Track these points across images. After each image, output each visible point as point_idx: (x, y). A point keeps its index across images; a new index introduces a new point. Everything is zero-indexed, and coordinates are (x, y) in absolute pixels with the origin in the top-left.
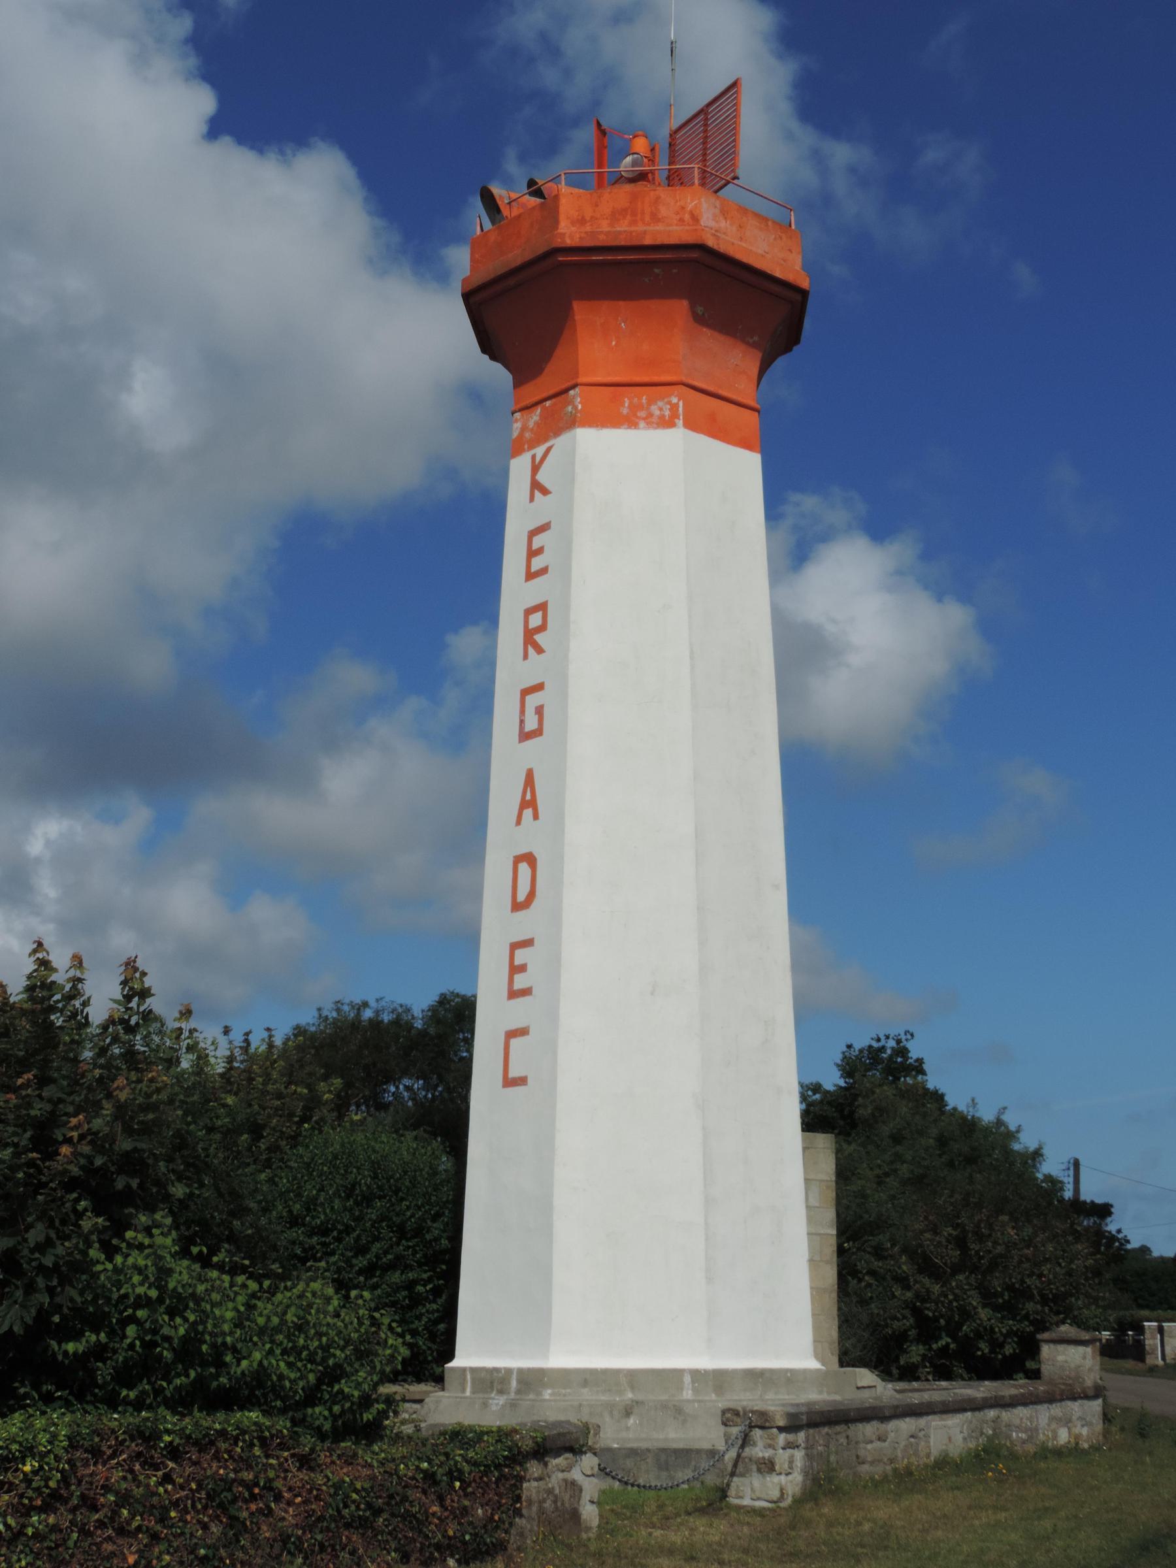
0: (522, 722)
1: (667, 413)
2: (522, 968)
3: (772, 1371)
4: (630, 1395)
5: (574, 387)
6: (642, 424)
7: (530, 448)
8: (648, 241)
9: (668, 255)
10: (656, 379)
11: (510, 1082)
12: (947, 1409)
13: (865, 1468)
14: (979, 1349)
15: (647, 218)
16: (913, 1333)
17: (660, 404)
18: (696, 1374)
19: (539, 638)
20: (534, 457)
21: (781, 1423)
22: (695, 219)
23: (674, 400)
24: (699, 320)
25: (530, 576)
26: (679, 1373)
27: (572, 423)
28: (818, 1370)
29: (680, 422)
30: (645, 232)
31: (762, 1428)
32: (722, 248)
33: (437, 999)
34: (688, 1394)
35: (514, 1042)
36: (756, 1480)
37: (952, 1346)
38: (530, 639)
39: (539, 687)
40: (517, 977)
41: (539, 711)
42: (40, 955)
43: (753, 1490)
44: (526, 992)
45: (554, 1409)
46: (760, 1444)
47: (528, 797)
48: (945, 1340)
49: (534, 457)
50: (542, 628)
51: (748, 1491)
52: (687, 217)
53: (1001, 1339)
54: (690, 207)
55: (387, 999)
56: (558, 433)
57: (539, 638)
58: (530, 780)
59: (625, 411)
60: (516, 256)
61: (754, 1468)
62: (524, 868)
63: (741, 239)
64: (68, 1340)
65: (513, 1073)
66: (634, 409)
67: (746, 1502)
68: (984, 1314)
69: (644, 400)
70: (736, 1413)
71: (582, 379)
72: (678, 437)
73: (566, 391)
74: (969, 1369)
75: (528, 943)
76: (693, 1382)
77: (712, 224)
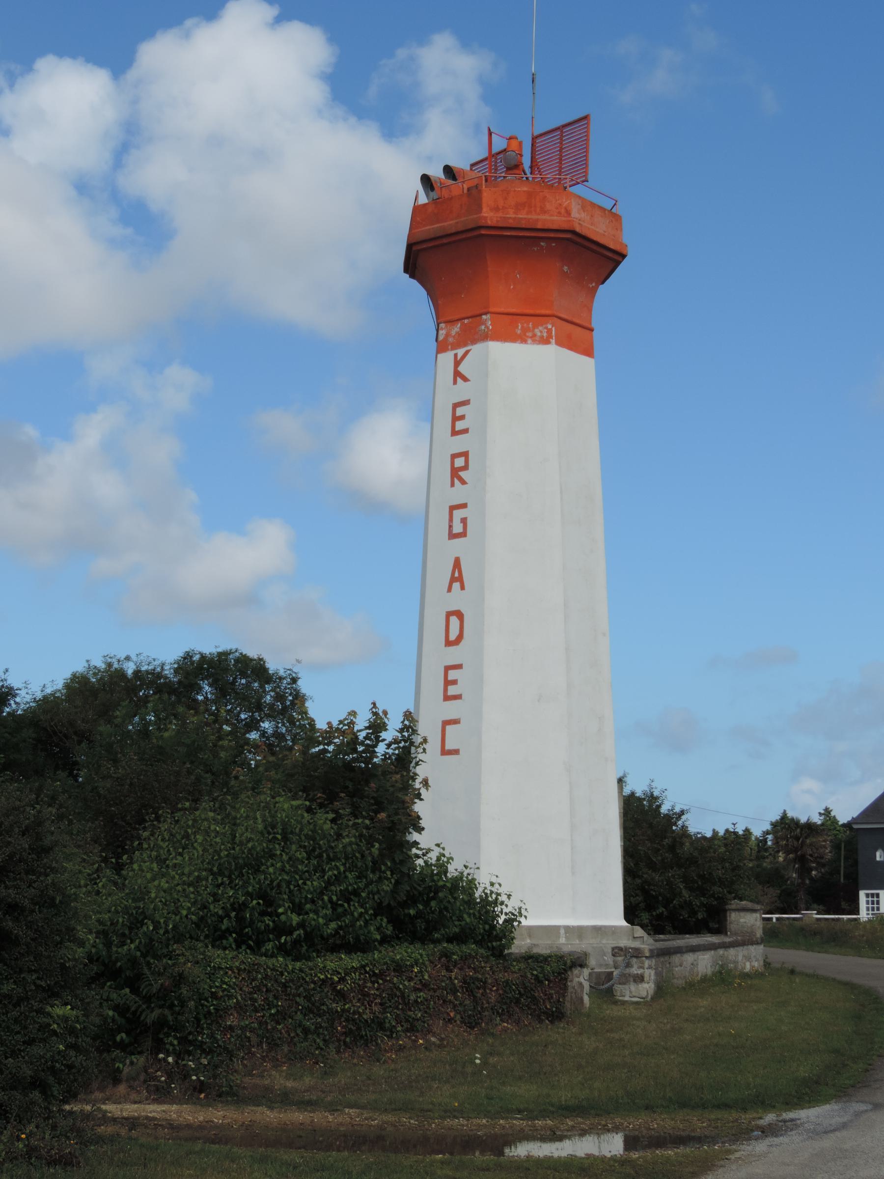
0: (450, 527)
1: (545, 335)
2: (455, 682)
3: (605, 927)
4: (529, 941)
5: (486, 314)
6: (529, 341)
7: (453, 349)
8: (539, 226)
9: (552, 235)
10: (538, 312)
11: (445, 752)
12: (693, 949)
13: (675, 981)
14: (681, 915)
15: (538, 210)
16: (642, 905)
17: (540, 328)
18: (567, 929)
19: (462, 474)
20: (456, 355)
21: (647, 955)
22: (568, 213)
23: (550, 326)
25: (454, 433)
26: (557, 928)
27: (485, 337)
28: (621, 927)
29: (553, 341)
30: (537, 220)
31: (637, 957)
32: (584, 232)
33: (182, 655)
34: (563, 940)
35: (448, 728)
36: (633, 987)
37: (665, 913)
39: (464, 506)
40: (450, 688)
41: (464, 521)
42: (374, 710)
43: (630, 992)
44: (458, 697)
45: (566, 945)
46: (635, 966)
47: (456, 575)
48: (661, 909)
49: (456, 355)
50: (465, 468)
51: (628, 993)
52: (563, 211)
53: (697, 909)
54: (565, 204)
55: (145, 655)
56: (474, 342)
57: (462, 474)
58: (457, 564)
59: (519, 332)
60: (450, 224)
61: (632, 979)
62: (454, 620)
63: (592, 224)
65: (448, 747)
66: (525, 330)
67: (627, 998)
68: (686, 894)
69: (530, 326)
70: (620, 949)
71: (492, 309)
72: (552, 351)
73: (481, 315)
74: (674, 928)
75: (459, 667)
76: (566, 933)
77: (577, 215)
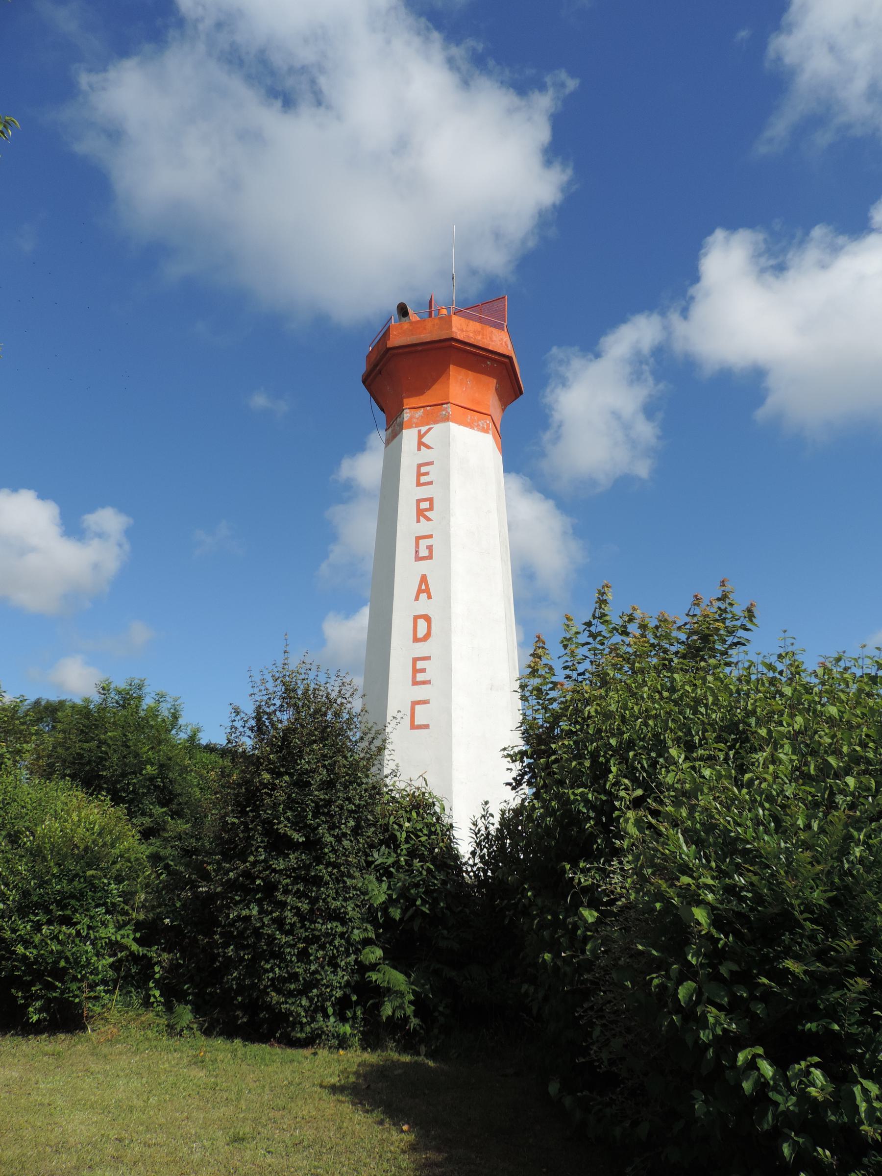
2: (423, 671)
5: (447, 403)
24: (496, 390)
27: (447, 419)
35: (418, 708)
38: (421, 514)
47: (423, 587)
56: (436, 422)
64: (827, 1073)
71: (452, 401)
